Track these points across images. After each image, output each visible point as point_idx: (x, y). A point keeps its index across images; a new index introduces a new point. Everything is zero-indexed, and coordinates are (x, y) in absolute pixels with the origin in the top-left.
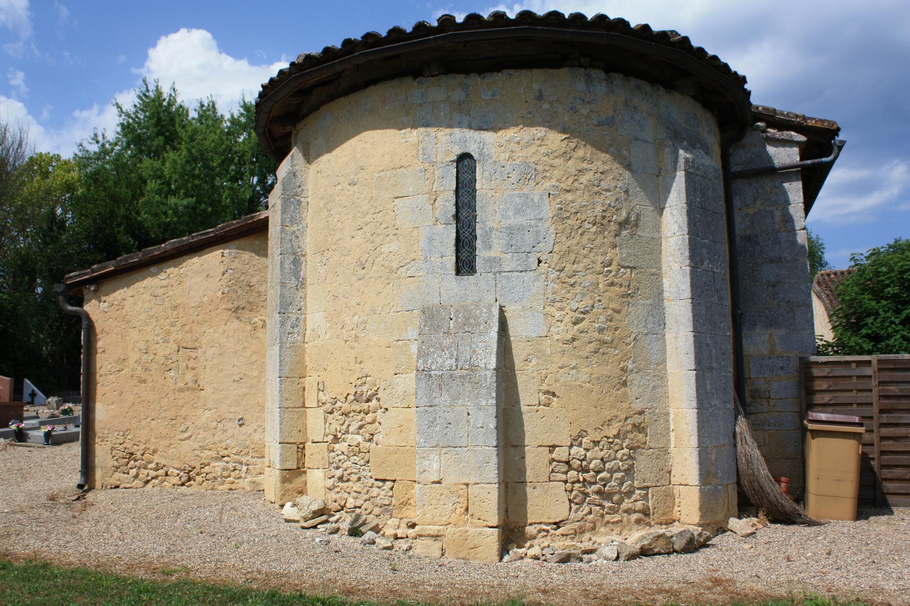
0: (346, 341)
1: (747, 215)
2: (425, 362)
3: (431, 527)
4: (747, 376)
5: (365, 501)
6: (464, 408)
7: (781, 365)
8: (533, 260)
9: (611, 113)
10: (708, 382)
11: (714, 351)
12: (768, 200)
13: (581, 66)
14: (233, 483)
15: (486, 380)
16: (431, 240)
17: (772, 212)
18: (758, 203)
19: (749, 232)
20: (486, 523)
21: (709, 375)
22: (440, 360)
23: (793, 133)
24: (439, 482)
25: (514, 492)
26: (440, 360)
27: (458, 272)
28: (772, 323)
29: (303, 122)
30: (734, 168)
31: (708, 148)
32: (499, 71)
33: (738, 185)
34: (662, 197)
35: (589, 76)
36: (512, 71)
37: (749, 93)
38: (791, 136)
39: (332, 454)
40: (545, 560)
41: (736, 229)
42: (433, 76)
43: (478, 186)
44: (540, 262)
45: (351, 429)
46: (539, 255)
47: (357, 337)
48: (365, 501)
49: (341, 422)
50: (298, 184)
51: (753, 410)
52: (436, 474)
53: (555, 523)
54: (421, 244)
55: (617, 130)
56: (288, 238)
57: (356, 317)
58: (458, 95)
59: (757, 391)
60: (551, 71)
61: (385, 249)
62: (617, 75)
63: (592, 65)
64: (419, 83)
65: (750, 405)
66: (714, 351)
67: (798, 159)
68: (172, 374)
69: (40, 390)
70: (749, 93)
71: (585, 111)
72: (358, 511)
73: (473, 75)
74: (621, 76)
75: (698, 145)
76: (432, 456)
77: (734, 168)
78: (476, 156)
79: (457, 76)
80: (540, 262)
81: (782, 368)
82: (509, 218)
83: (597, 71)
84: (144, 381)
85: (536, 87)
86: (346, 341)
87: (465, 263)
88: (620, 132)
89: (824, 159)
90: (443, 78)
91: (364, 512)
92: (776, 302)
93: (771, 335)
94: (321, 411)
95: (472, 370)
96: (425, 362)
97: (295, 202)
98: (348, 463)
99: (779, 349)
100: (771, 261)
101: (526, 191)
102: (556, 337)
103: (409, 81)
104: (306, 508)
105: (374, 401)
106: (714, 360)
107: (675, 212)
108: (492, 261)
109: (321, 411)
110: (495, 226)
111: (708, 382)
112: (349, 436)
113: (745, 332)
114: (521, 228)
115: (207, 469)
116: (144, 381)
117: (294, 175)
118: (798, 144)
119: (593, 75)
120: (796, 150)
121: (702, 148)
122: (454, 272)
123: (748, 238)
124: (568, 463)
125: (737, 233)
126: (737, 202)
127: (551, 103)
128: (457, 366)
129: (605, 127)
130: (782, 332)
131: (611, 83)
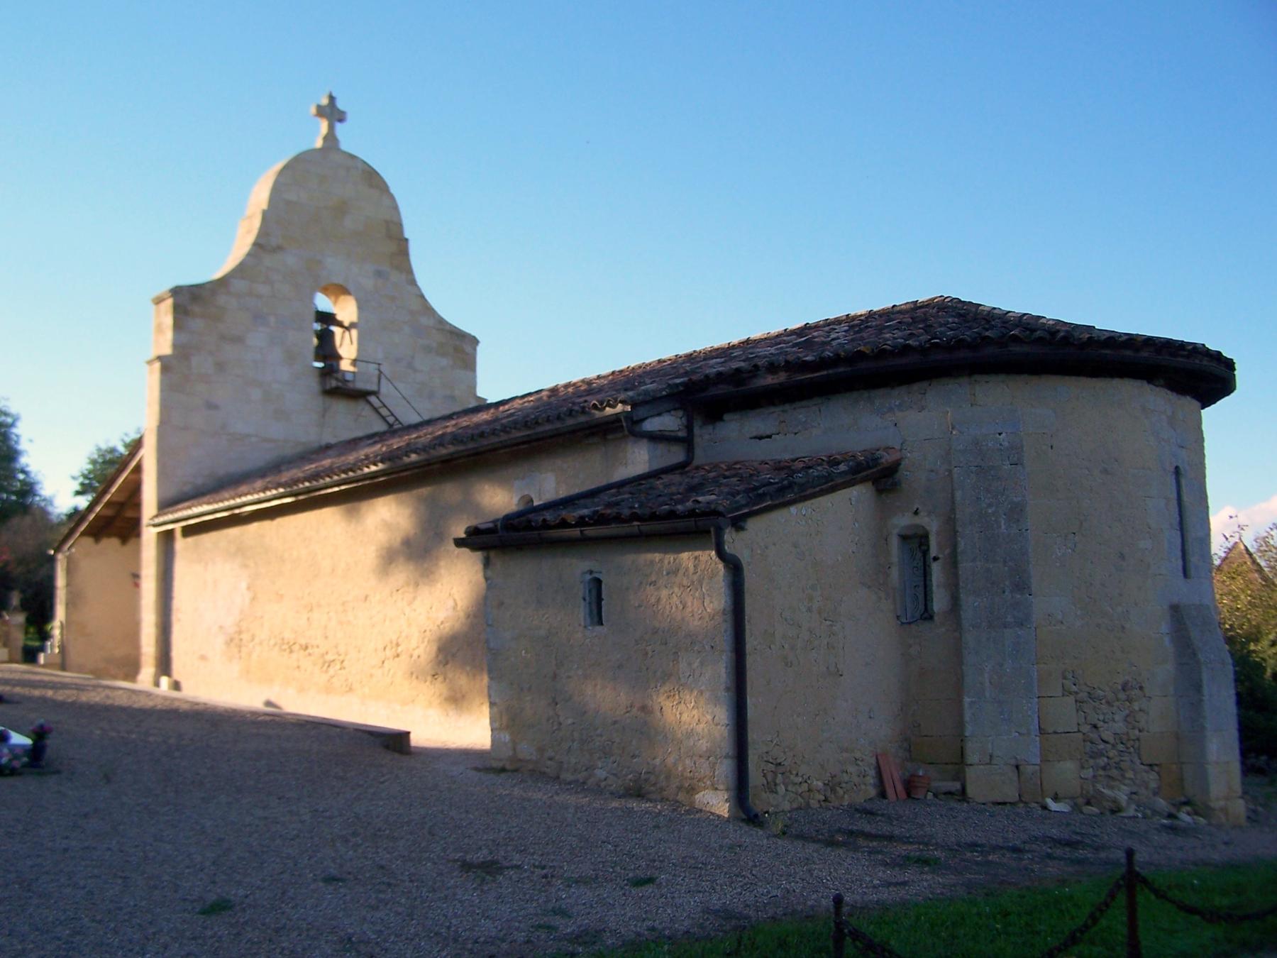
94: (1071, 699)
109: (1071, 699)
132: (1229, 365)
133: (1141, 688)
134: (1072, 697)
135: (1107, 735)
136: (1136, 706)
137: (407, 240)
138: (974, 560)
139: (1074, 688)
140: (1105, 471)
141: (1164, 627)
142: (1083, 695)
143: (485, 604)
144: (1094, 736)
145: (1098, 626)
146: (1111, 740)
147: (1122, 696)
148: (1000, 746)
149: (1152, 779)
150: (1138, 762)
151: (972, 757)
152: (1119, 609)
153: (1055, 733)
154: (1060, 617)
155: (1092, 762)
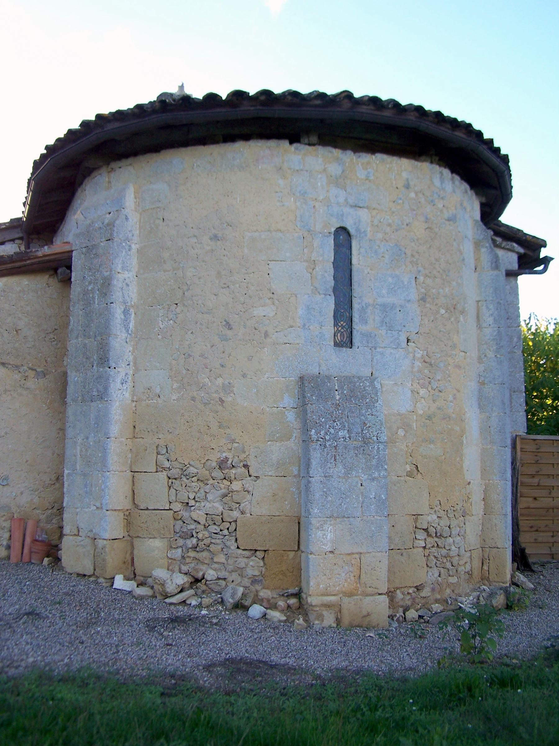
6: (357, 479)
8: (403, 339)
16: (309, 308)
20: (376, 591)
23: (515, 245)
24: (331, 552)
29: (119, 164)
38: (514, 247)
42: (310, 145)
43: (354, 261)
44: (408, 341)
52: (329, 545)
54: (300, 312)
58: (334, 169)
64: (296, 149)
76: (326, 527)
78: (352, 231)
85: (405, 175)
87: (345, 339)
94: (163, 476)
97: (127, 247)
101: (397, 272)
102: (421, 412)
107: (491, 307)
108: (368, 336)
109: (163, 476)
110: (371, 302)
114: (393, 306)
118: (518, 253)
120: (515, 257)
127: (416, 193)
132: (545, 241)
133: (246, 466)
134: (165, 473)
135: (199, 515)
136: (236, 486)
137: (11, 220)
138: (77, 338)
139: (167, 464)
140: (215, 238)
141: (288, 401)
142: (175, 472)
143: (542, 432)
144: (185, 514)
145: (193, 399)
146: (203, 521)
147: (218, 474)
148: (95, 518)
149: (254, 566)
150: (233, 546)
151: (66, 530)
152: (220, 381)
153: (147, 509)
154: (158, 391)
155: (181, 542)
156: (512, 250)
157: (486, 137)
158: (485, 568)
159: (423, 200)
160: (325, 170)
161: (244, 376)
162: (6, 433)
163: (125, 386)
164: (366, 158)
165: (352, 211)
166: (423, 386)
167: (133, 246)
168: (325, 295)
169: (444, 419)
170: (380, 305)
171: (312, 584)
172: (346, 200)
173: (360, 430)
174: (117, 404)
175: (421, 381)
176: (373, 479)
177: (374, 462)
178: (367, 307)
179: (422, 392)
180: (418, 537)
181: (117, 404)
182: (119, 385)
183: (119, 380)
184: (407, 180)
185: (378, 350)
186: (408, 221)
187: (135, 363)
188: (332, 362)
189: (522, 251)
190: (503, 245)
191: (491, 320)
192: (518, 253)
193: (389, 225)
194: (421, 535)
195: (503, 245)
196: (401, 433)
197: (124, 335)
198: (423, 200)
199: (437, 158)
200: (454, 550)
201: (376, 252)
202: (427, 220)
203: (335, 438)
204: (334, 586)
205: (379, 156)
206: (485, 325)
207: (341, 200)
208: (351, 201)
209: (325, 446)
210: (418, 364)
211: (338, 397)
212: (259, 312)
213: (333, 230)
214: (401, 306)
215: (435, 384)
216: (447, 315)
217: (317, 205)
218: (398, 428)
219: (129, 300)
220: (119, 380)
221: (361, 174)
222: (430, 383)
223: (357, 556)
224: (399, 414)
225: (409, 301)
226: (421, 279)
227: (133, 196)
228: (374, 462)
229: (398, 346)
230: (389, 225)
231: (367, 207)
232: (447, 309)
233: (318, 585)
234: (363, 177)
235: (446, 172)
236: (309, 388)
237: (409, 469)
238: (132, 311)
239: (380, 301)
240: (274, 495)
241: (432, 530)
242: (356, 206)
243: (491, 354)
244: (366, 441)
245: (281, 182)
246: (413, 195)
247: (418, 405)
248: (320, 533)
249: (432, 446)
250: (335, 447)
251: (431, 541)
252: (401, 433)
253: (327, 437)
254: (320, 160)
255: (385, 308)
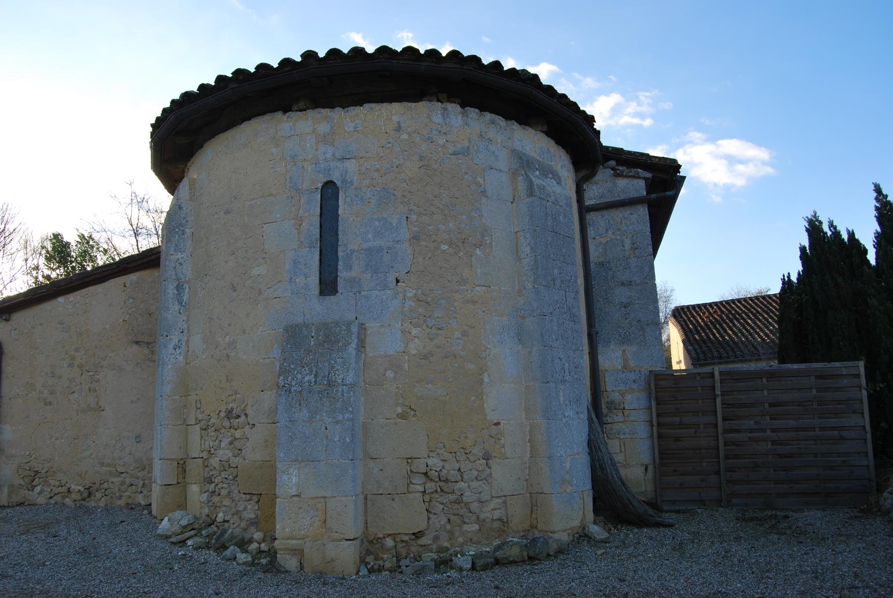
0: (219, 361)
1: (601, 243)
2: (286, 378)
3: (289, 541)
4: (603, 389)
5: (233, 515)
7: (634, 378)
8: (391, 279)
9: (466, 144)
10: (561, 394)
11: (567, 365)
12: (619, 230)
13: (438, 101)
14: (130, 497)
15: (343, 395)
16: (295, 262)
17: (622, 241)
18: (610, 232)
19: (602, 259)
20: (343, 536)
21: (563, 387)
22: (299, 376)
24: (298, 496)
25: (373, 504)
26: (299, 376)
27: (322, 293)
28: (625, 340)
30: (588, 202)
31: (560, 178)
32: (361, 105)
33: (591, 217)
34: (690, 348)
35: (445, 109)
36: (373, 105)
37: (599, 132)
39: (207, 469)
40: (401, 572)
41: (591, 256)
42: (301, 110)
43: (340, 212)
44: (398, 281)
45: (223, 445)
46: (397, 275)
47: (228, 356)
48: (233, 515)
49: (214, 439)
50: (183, 216)
51: (609, 420)
52: (295, 488)
53: (414, 534)
54: (287, 267)
55: (472, 159)
56: (173, 265)
57: (227, 338)
58: (323, 128)
59: (612, 402)
60: (409, 104)
61: (255, 272)
62: (472, 109)
63: (450, 99)
65: (607, 416)
66: (567, 365)
67: (645, 193)
68: (76, 395)
69: (870, 416)
70: (599, 132)
71: (441, 141)
72: (226, 525)
73: (337, 109)
74: (477, 110)
75: (550, 176)
76: (291, 470)
77: (588, 202)
78: (339, 183)
79: (323, 110)
80: (398, 281)
81: (634, 381)
82: (369, 241)
83: (454, 105)
84: (50, 403)
85: (395, 118)
86: (219, 361)
87: (328, 285)
88: (475, 162)
89: (668, 193)
90: (310, 113)
91: (232, 526)
92: (627, 321)
93: (624, 351)
94: (198, 427)
95: (329, 385)
96: (286, 378)
97: (180, 232)
98: (219, 478)
99: (632, 363)
100: (623, 284)
102: (414, 352)
103: (279, 115)
104: (176, 523)
105: (243, 417)
106: (567, 373)
107: (528, 236)
109: (198, 427)
110: (356, 248)
111: (561, 394)
112: (221, 452)
113: (600, 349)
114: (380, 249)
115: (105, 485)
116: (50, 403)
117: (180, 208)
118: (645, 179)
119: (450, 109)
120: (642, 183)
121: (553, 178)
122: (317, 292)
123: (601, 264)
124: (426, 474)
125: (591, 259)
126: (591, 232)
127: (409, 134)
128: (315, 382)
129: (460, 156)
130: (634, 348)
131: (467, 116)
147: (226, 423)
156: (637, 177)
157: (486, 61)
158: (534, 516)
159: (418, 139)
160: (314, 130)
161: (244, 332)
162: (138, 399)
163: (178, 351)
164: (354, 111)
165: (339, 164)
166: (416, 326)
167: (187, 231)
168: (310, 247)
169: (446, 357)
170: (366, 250)
171: (278, 527)
172: (334, 155)
173: (327, 373)
174: (170, 367)
175: (414, 321)
176: (337, 423)
177: (339, 405)
178: (352, 254)
179: (414, 332)
180: (414, 481)
181: (170, 367)
182: (171, 351)
183: (171, 347)
184: (399, 123)
185: (363, 293)
186: (397, 163)
187: (189, 331)
188: (314, 308)
189: (648, 175)
190: (625, 173)
191: (528, 249)
192: (645, 179)
193: (378, 170)
194: (418, 480)
195: (625, 173)
196: (390, 374)
197: (177, 307)
198: (418, 139)
199: (445, 95)
200: (468, 496)
201: (362, 199)
202: (421, 158)
203: (301, 384)
204: (299, 530)
205: (367, 106)
206: (523, 256)
207: (329, 156)
208: (338, 155)
209: (290, 392)
210: (409, 303)
211: (312, 343)
212: (255, 272)
213: (320, 185)
214: (389, 248)
215: (431, 322)
216: (451, 250)
217: (305, 164)
218: (386, 370)
219: (182, 277)
220: (171, 347)
221: (349, 127)
222: (424, 321)
223: (323, 500)
224: (386, 356)
225: (399, 241)
226: (414, 217)
227: (187, 187)
228: (339, 405)
229: (385, 287)
230: (378, 170)
231: (355, 158)
232: (451, 244)
233: (284, 529)
234: (352, 129)
235: (454, 108)
236: (294, 335)
237: (400, 411)
238: (186, 286)
239: (365, 245)
240: (266, 441)
241: (433, 474)
242: (343, 159)
243: (529, 285)
244: (331, 384)
245: (274, 150)
246: (405, 136)
247: (411, 345)
248: (285, 477)
249: (430, 386)
250: (300, 392)
251: (431, 487)
252: (390, 374)
253: (293, 384)
254: (310, 123)
255: (371, 252)
